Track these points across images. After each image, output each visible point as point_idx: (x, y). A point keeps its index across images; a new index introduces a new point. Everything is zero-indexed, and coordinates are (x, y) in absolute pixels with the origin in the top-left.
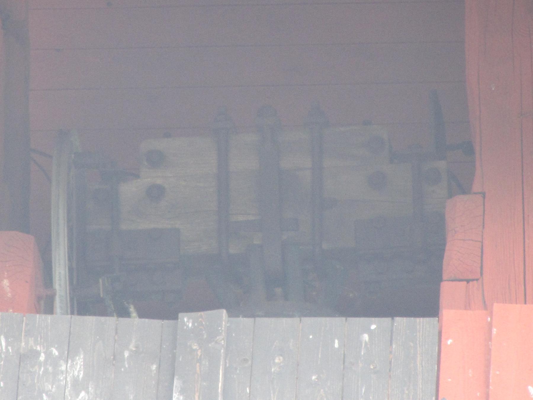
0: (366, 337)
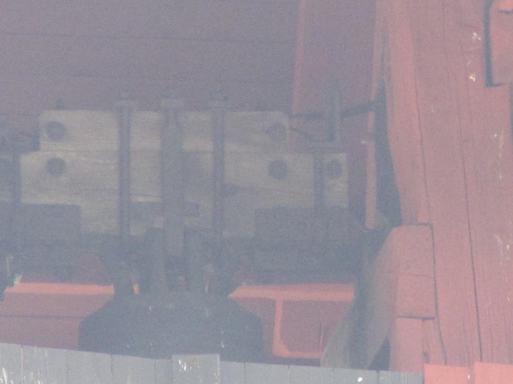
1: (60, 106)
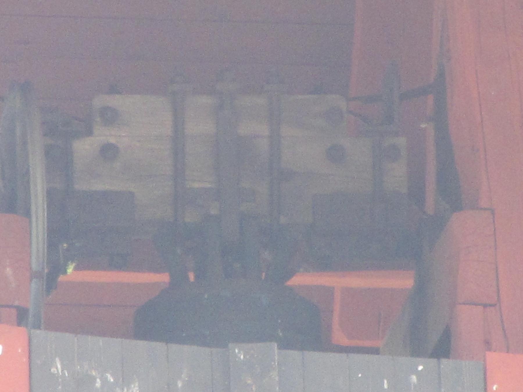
0: (414, 378)
1: (113, 90)
